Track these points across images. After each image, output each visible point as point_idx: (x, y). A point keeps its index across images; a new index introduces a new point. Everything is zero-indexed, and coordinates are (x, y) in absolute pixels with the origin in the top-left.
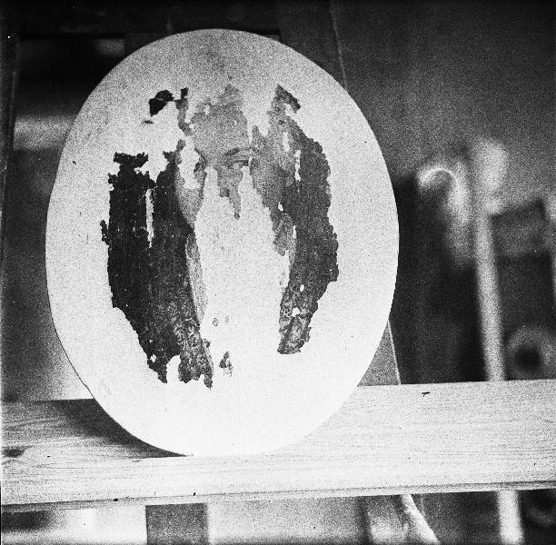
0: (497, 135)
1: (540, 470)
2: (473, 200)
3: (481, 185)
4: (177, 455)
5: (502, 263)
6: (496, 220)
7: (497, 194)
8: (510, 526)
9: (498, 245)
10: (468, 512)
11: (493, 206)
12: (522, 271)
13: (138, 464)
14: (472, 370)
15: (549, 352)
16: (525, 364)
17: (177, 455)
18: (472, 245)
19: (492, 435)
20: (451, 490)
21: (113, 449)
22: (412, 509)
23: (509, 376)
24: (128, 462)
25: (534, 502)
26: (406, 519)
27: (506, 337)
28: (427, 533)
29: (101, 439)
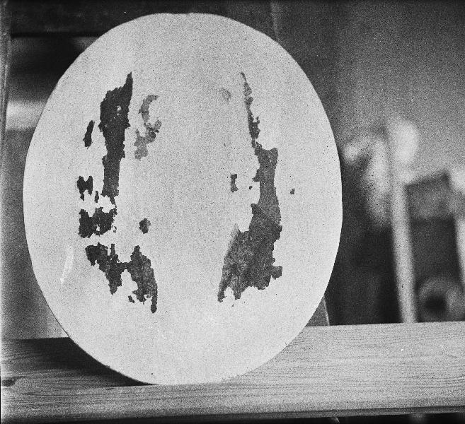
0: (410, 116)
2: (391, 174)
3: (410, 152)
5: (415, 224)
6: (410, 190)
9: (411, 209)
11: (408, 177)
12: (434, 232)
13: (111, 391)
14: (390, 313)
15: (454, 300)
16: (432, 309)
18: (389, 212)
19: (418, 357)
23: (420, 319)
24: (103, 390)
27: (417, 286)
29: (73, 372)
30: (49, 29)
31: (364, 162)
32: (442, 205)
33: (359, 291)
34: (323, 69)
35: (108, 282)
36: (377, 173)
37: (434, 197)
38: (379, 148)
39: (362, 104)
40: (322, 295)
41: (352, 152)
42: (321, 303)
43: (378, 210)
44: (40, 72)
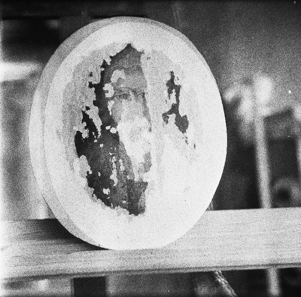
0: (268, 71)
1: (290, 256)
2: (255, 109)
3: (261, 97)
4: (107, 249)
5: (271, 143)
6: (268, 120)
7: (269, 105)
8: (274, 288)
9: (268, 133)
10: (249, 282)
11: (266, 112)
12: (282, 148)
14: (253, 202)
15: (295, 192)
16: (282, 199)
17: (49, 208)
20: (249, 268)
21: (93, 253)
22: (222, 280)
23: (274, 205)
25: (288, 274)
26: (218, 284)
27: (272, 183)
28: (230, 291)
30: (27, 14)
31: (236, 102)
32: (288, 129)
33: (237, 190)
34: (218, 67)
35: (177, 128)
36: (245, 110)
37: (282, 126)
38: (246, 93)
39: (237, 57)
40: (210, 200)
41: (230, 95)
42: (210, 205)
43: (245, 130)
44: (37, 41)
